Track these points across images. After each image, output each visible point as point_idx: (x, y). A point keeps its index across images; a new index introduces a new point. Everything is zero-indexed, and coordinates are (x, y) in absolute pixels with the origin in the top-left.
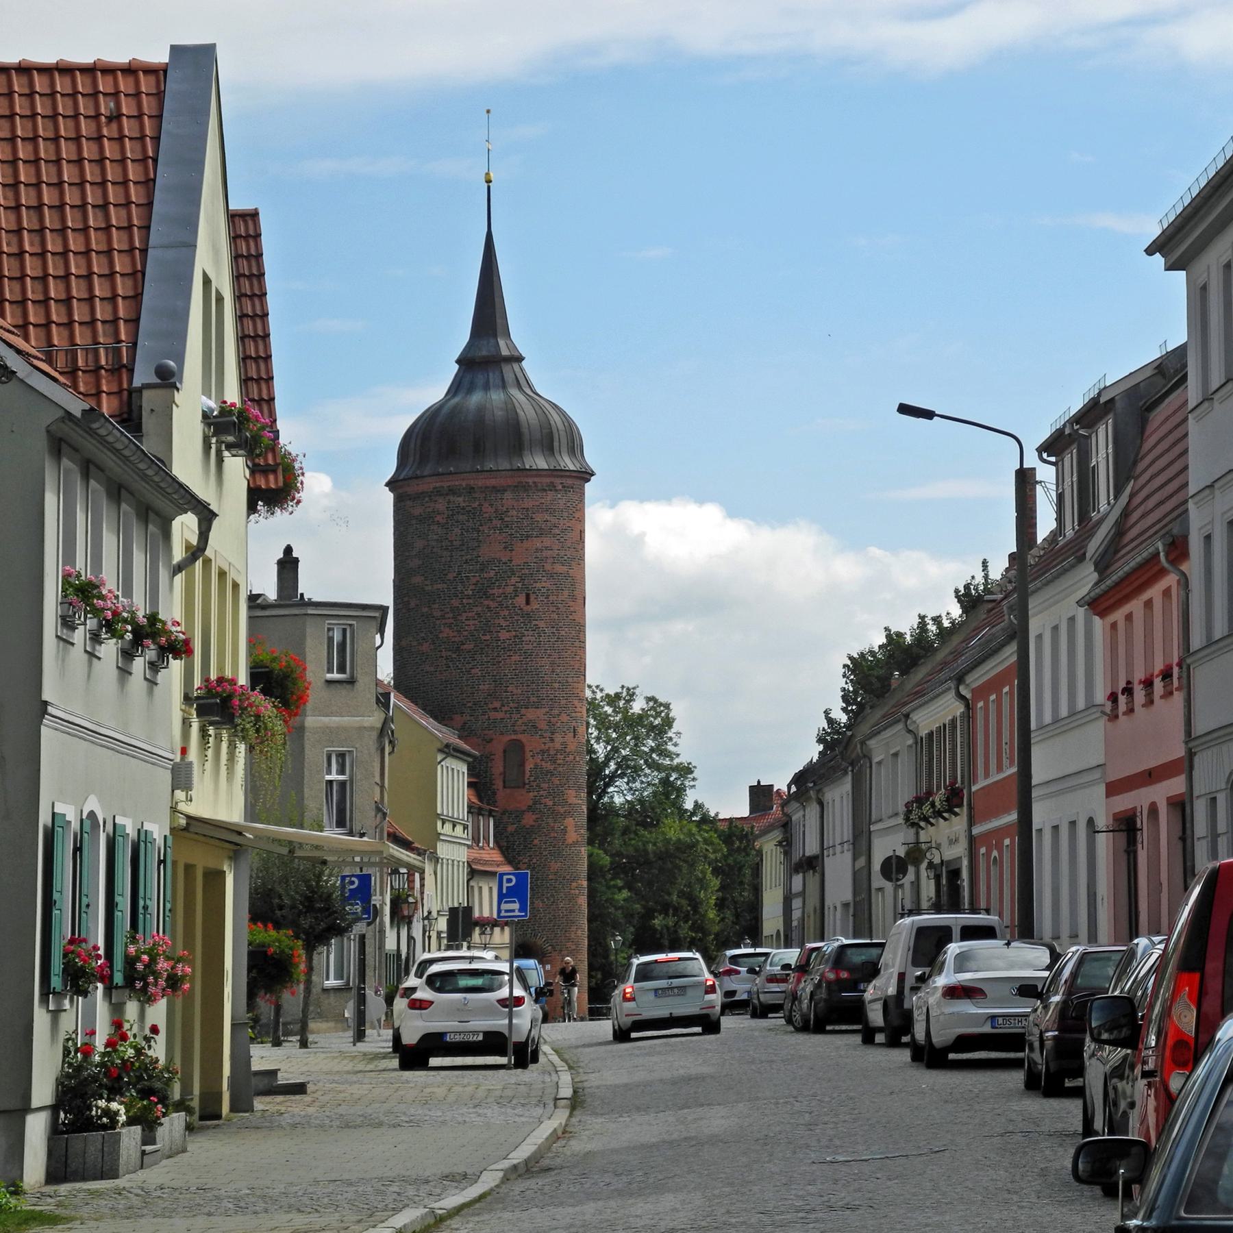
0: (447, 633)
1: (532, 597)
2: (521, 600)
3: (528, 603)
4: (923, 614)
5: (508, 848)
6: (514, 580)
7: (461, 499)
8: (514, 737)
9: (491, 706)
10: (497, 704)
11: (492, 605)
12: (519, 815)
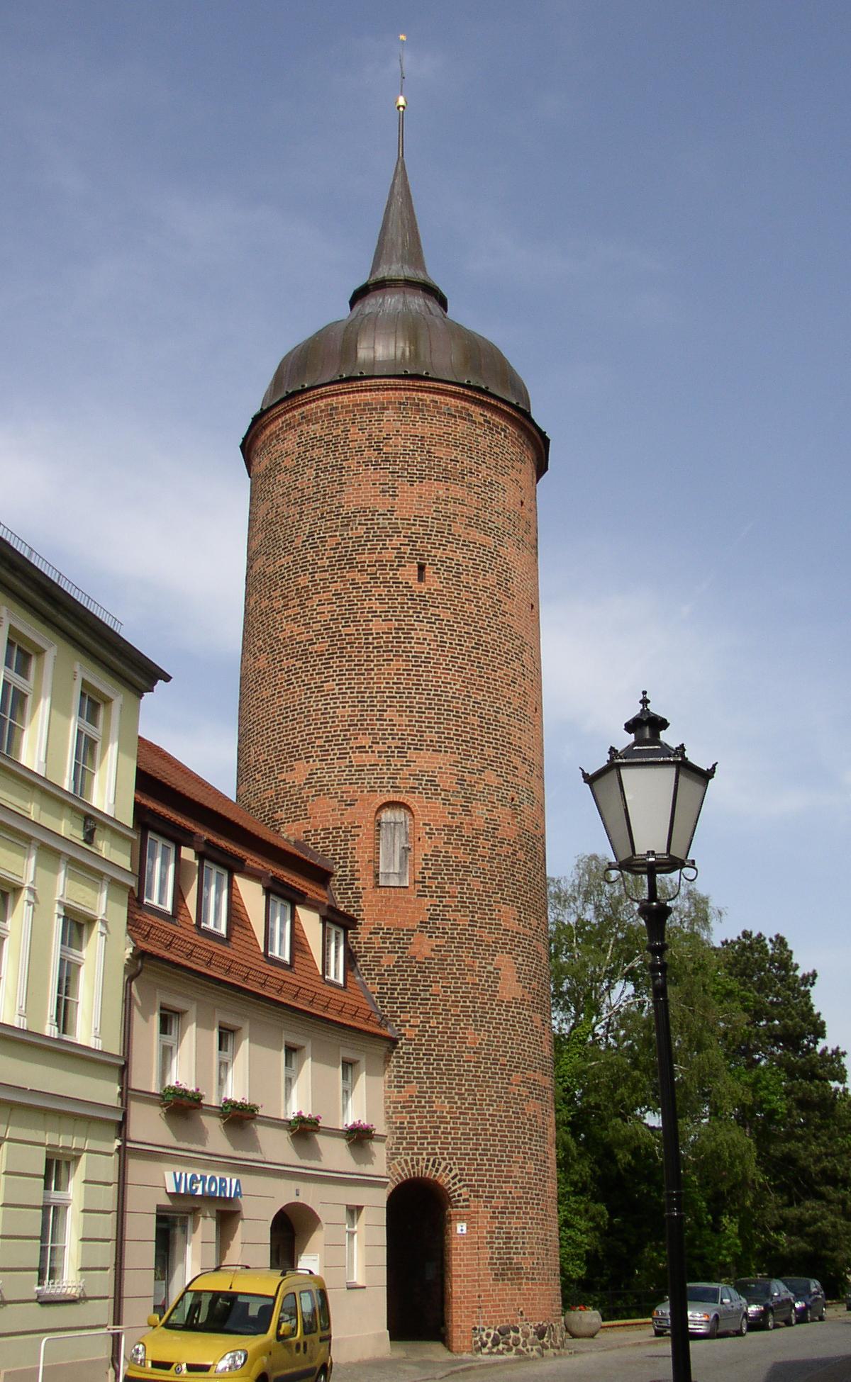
0: (290, 628)
1: (429, 571)
2: (409, 573)
4: (818, 972)
5: (382, 996)
6: (396, 541)
7: (317, 426)
8: (395, 797)
9: (353, 743)
10: (366, 741)
12: (399, 937)
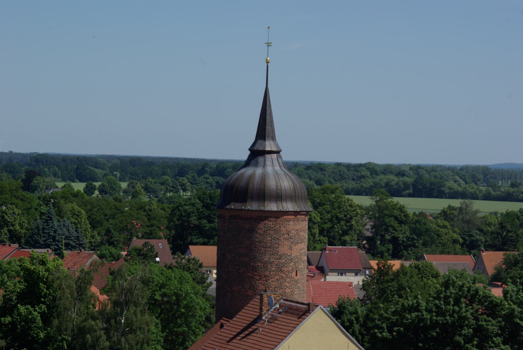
1: (298, 272)
2: (294, 273)
3: (296, 275)
6: (292, 264)
11: (284, 276)
